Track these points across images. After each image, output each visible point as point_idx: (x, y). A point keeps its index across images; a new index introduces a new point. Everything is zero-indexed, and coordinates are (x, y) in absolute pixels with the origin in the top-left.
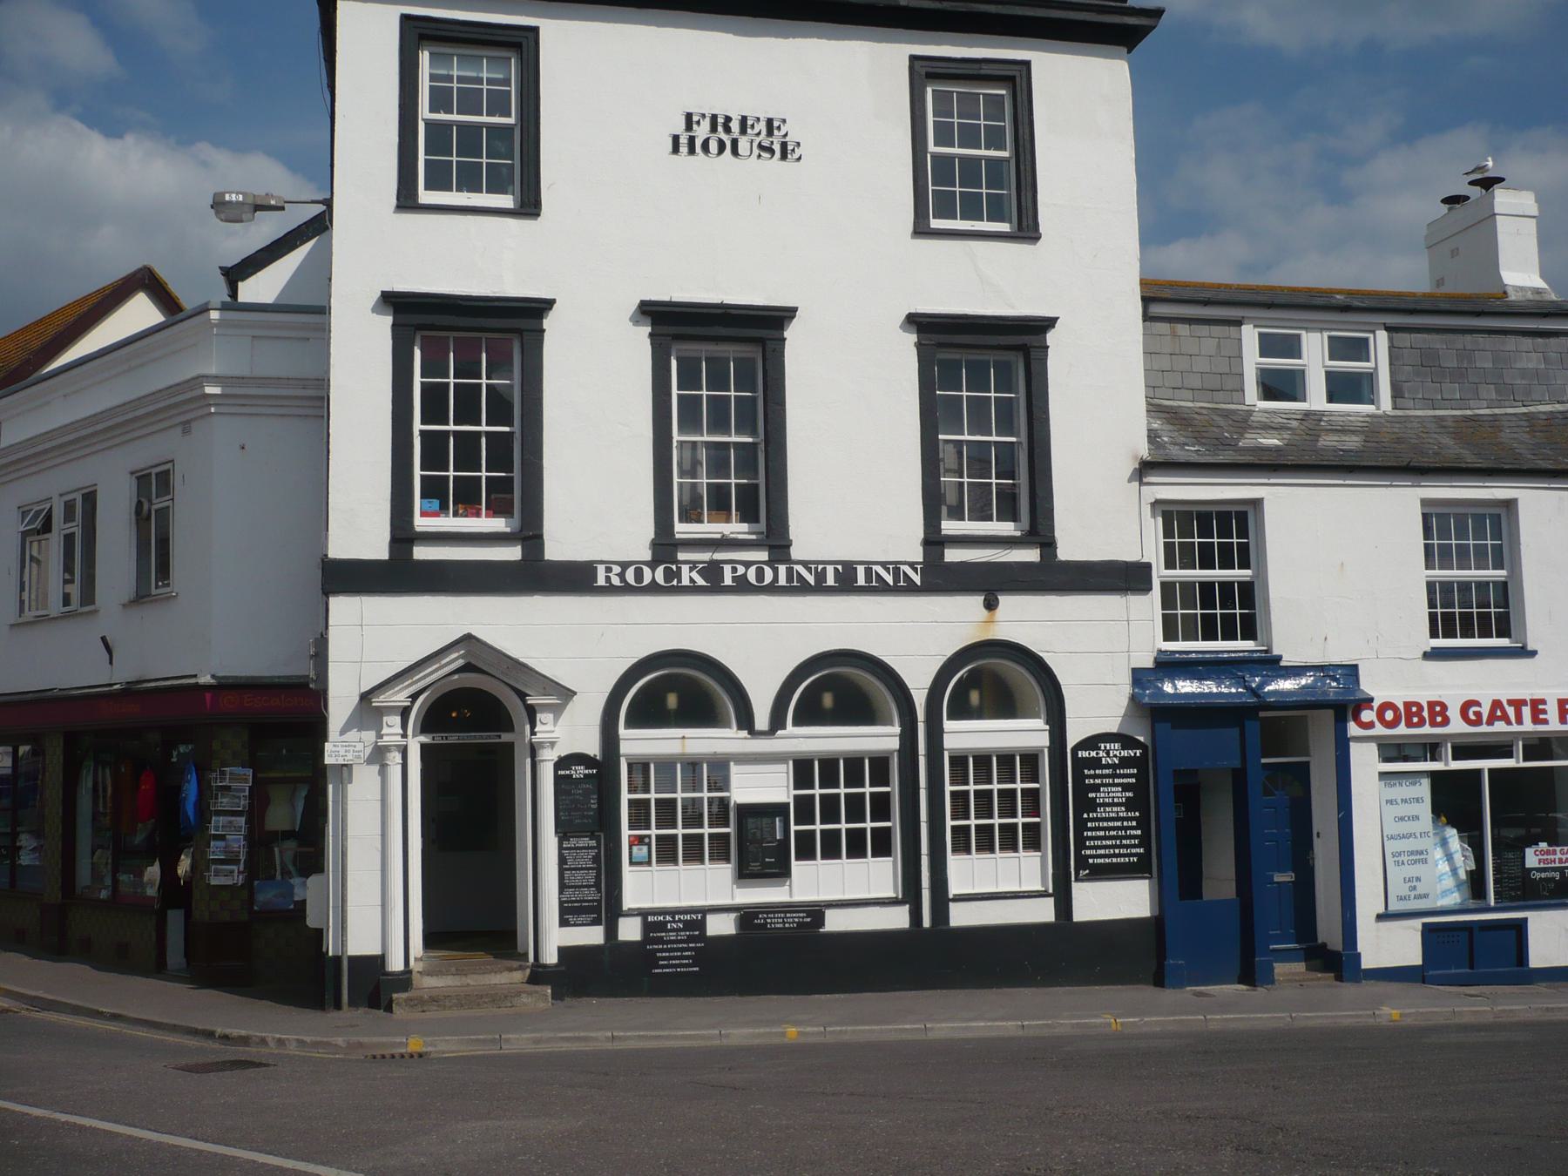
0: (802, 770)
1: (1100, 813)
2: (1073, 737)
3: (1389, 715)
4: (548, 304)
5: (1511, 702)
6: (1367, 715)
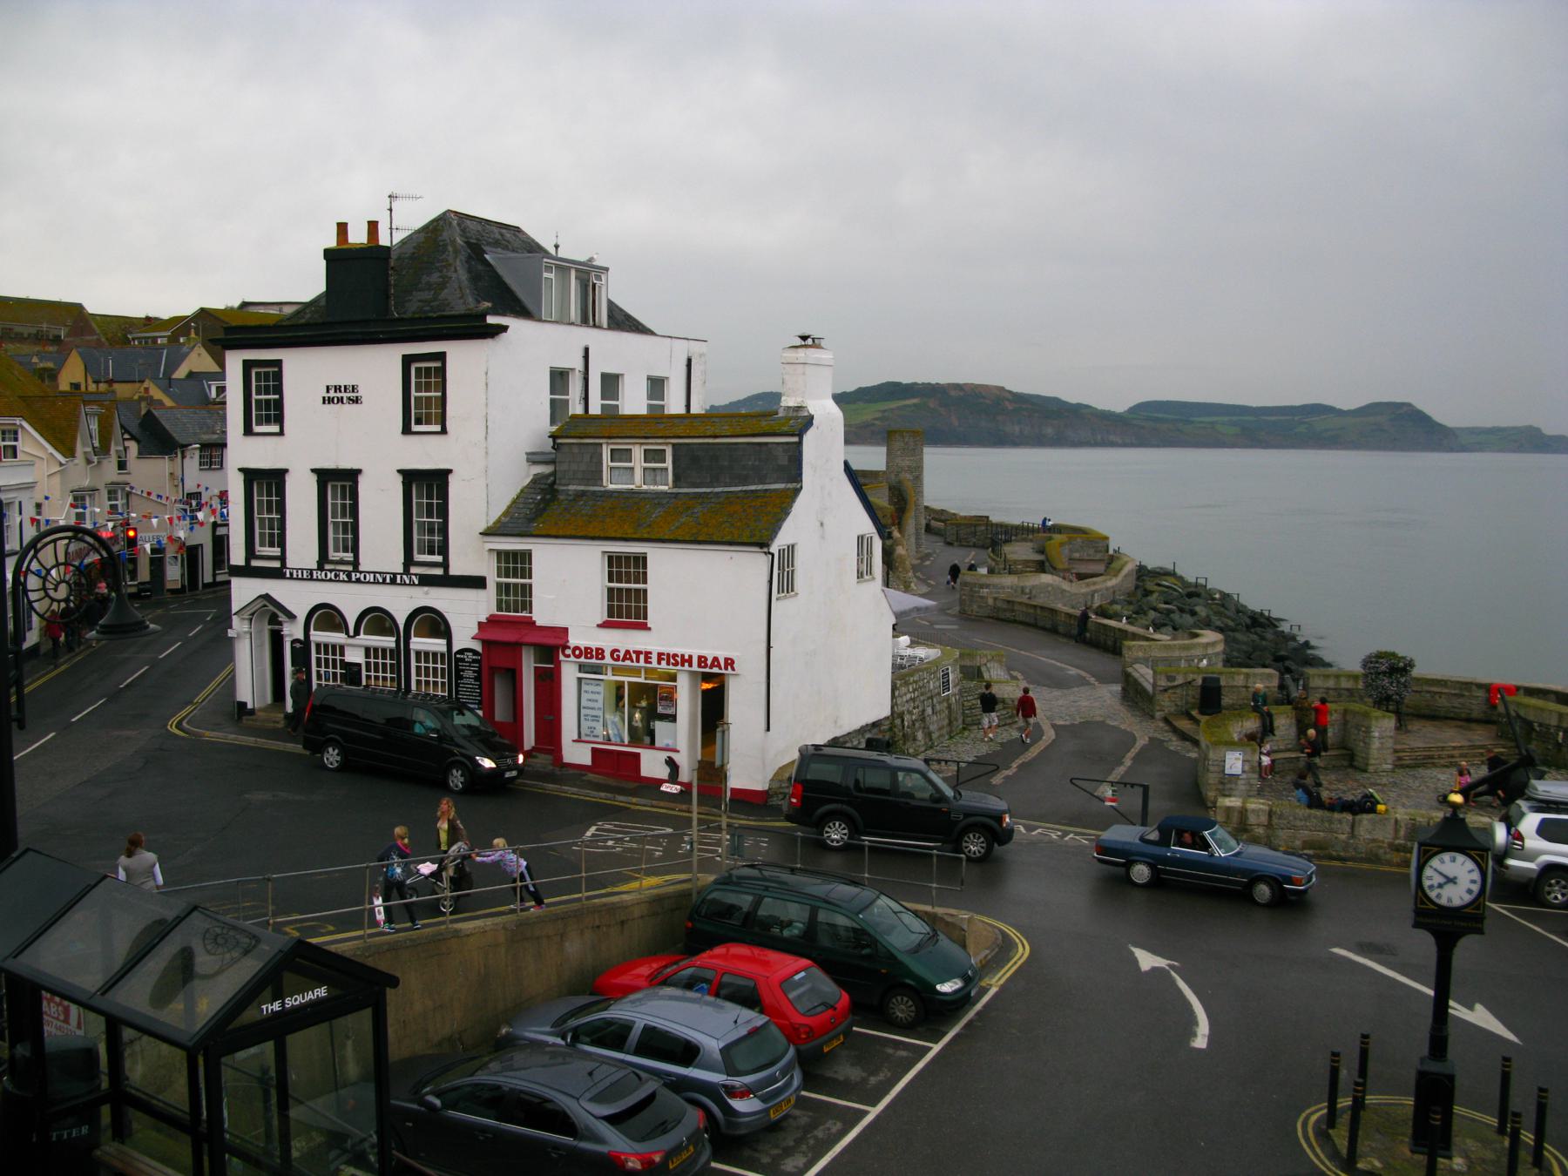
0: (367, 650)
1: (465, 681)
2: (455, 648)
3: (577, 652)
4: (450, 471)
5: (635, 652)
6: (568, 652)
